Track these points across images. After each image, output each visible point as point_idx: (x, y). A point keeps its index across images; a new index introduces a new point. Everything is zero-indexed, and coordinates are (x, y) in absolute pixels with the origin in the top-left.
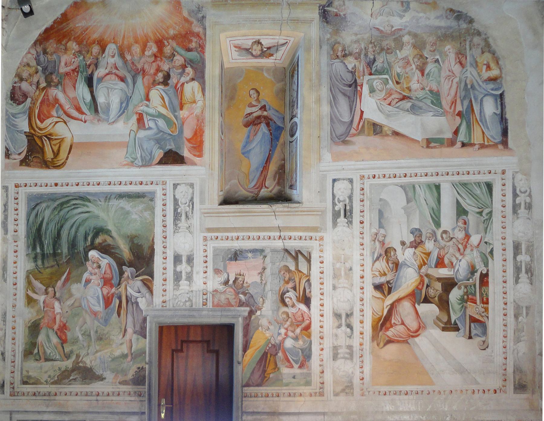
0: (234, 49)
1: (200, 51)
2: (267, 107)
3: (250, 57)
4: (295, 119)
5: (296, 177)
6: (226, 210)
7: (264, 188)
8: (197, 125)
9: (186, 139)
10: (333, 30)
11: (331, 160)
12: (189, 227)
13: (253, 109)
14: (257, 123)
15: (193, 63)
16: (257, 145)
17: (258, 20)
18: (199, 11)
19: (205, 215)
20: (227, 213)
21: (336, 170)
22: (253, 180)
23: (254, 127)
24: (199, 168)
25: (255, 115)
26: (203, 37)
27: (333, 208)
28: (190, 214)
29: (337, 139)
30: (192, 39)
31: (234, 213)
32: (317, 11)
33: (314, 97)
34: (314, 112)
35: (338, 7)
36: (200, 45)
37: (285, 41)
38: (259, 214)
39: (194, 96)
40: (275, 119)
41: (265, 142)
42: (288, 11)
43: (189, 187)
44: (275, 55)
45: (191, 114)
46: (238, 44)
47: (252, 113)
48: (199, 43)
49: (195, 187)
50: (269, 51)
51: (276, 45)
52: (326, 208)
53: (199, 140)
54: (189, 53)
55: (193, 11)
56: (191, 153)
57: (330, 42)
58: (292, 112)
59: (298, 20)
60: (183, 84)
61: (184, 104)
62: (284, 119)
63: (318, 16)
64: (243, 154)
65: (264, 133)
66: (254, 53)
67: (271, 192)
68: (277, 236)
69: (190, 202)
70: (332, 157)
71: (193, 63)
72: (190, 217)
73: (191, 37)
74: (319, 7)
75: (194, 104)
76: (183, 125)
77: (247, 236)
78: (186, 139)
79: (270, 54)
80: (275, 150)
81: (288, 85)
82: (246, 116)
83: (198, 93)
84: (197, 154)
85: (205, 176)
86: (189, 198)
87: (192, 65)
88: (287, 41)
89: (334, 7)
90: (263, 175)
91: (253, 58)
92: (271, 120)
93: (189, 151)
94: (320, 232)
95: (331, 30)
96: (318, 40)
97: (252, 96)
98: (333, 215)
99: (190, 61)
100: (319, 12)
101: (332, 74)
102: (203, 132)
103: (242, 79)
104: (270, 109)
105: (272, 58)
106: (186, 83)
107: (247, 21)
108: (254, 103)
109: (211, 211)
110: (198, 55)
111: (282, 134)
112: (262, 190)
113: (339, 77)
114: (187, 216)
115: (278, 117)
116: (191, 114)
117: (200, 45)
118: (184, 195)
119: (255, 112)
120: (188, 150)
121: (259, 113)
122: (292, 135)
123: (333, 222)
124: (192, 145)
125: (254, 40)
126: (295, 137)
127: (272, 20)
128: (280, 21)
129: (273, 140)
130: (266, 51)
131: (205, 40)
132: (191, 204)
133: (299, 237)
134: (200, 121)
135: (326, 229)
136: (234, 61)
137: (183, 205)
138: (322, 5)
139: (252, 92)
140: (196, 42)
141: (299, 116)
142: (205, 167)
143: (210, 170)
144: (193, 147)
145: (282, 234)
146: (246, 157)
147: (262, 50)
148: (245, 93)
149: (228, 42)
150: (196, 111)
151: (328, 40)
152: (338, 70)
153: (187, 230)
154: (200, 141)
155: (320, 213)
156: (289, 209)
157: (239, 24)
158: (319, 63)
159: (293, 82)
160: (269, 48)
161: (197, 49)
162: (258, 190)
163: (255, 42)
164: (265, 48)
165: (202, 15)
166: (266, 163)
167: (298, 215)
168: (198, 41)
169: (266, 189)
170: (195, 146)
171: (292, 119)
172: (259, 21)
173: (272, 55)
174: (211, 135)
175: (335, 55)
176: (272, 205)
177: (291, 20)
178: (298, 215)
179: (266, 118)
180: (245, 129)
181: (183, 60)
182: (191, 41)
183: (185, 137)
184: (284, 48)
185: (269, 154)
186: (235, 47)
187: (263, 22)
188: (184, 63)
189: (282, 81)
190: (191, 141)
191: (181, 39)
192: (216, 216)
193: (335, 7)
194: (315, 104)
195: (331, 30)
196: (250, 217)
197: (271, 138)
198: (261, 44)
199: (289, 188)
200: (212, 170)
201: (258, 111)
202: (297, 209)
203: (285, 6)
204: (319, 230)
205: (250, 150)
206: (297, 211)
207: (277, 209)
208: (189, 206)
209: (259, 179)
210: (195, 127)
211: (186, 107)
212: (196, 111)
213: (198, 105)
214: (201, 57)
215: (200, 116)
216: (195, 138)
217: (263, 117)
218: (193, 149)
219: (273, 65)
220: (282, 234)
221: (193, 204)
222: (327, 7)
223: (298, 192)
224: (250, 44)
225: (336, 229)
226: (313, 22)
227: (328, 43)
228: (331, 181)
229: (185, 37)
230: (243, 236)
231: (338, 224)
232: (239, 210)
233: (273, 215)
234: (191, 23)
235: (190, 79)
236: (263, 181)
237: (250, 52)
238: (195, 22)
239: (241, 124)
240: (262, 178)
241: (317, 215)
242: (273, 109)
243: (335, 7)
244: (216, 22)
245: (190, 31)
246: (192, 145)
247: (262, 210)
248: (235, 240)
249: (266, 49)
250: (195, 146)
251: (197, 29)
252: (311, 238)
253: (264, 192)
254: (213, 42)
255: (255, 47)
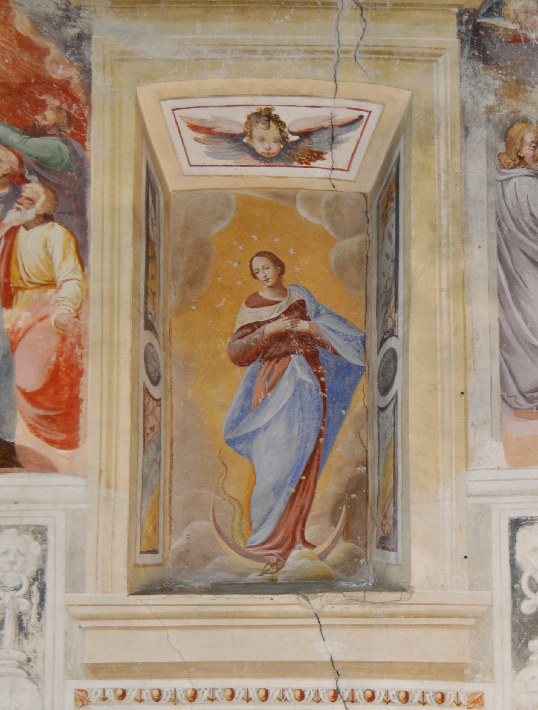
0: (189, 135)
1: (72, 135)
2: (310, 308)
3: (248, 159)
4: (392, 343)
5: (395, 511)
6: (155, 610)
7: (299, 545)
8: (60, 353)
9: (24, 393)
10: (505, 82)
11: (502, 461)
12: (29, 660)
13: (265, 313)
14: (277, 353)
15: (49, 171)
16: (277, 416)
17: (260, 49)
18: (69, 18)
19: (84, 624)
20: (158, 617)
21: (522, 493)
22: (261, 524)
23: (266, 367)
24: (66, 479)
25: (269, 329)
26: (81, 95)
27: (515, 606)
28: (31, 621)
29: (521, 400)
30: (44, 101)
31: (180, 617)
32: (453, 28)
33: (444, 276)
34: (445, 317)
35: (522, 17)
36: (70, 117)
37: (355, 115)
38: (269, 622)
39: (50, 266)
40: (337, 343)
41: (302, 409)
42: (358, 26)
43: (29, 537)
44: (327, 156)
45: (42, 319)
46: (202, 120)
47: (259, 324)
48: (68, 114)
49: (50, 536)
50: (305, 144)
51: (328, 124)
52: (491, 606)
53: (66, 396)
54: (35, 140)
55: (48, 19)
56: (38, 436)
57: (496, 117)
58: (385, 322)
59: (390, 53)
60: (13, 232)
61: (18, 288)
62: (364, 343)
63: (457, 41)
64: (231, 443)
65: (300, 384)
66: (260, 148)
67: (322, 557)
68: (328, 691)
69: (31, 584)
70: (507, 453)
71: (49, 171)
72: (30, 629)
73: (41, 94)
74: (460, 15)
75: (50, 292)
76: (13, 351)
77: (225, 690)
78: (24, 393)
79: (312, 152)
80: (335, 431)
81: (374, 243)
82: (240, 333)
83: (64, 258)
84: (62, 437)
85: (84, 506)
86: (31, 570)
87: (44, 174)
88: (361, 113)
89: (506, 17)
90: (296, 510)
91: (257, 162)
92: (323, 345)
93: (33, 429)
94: (472, 679)
95: (498, 83)
96: (458, 114)
97: (260, 276)
98: (515, 628)
99: (37, 163)
100: (459, 32)
101: (505, 210)
102: (81, 373)
103: (225, 224)
104: (317, 314)
105: (318, 163)
106: (22, 230)
107: (225, 51)
108: (266, 294)
109: (106, 611)
110: (65, 148)
111: (359, 387)
112: (295, 553)
113: (528, 218)
114: (21, 627)
115: (346, 338)
116: (42, 319)
117: (70, 117)
118: (13, 563)
119: (269, 322)
120: (30, 425)
121: (284, 324)
122: (385, 390)
123: (513, 649)
124: (41, 412)
125: (254, 110)
126: (391, 394)
127: (306, 52)
128: (332, 53)
129: (328, 405)
130: (296, 142)
131: (88, 103)
132: (35, 588)
133: (402, 695)
134: (70, 340)
135: (492, 671)
136: (196, 171)
137: (10, 594)
138: (467, 11)
139: (259, 263)
140: (59, 108)
141: (400, 333)
142: (85, 477)
143: (103, 486)
144: (45, 417)
145: (344, 684)
146: (240, 453)
147: (284, 139)
148: (235, 265)
149: (168, 114)
150: (57, 312)
151: (490, 110)
152: (523, 200)
153: (20, 671)
154: (70, 398)
155: (471, 622)
156: (367, 609)
157: (197, 59)
158: (463, 178)
159: (386, 233)
160: (306, 134)
161: (60, 131)
162: (280, 551)
163: (258, 115)
164: (293, 134)
165: (77, 31)
166: (307, 472)
167: (396, 626)
168: (65, 107)
169: (306, 550)
170: (51, 413)
171: (383, 341)
172: (265, 52)
173: (319, 156)
174: (105, 381)
175: (514, 155)
176: (310, 596)
177: (369, 52)
178: (396, 626)
179: (303, 337)
180: (238, 369)
181: (13, 158)
182: (43, 106)
183: (19, 388)
184: (353, 135)
185: (318, 444)
186: (194, 128)
187: (276, 56)
188: (16, 167)
189: (358, 231)
190: (40, 399)
191: (9, 99)
192: (120, 628)
193: (512, 16)
194: (448, 296)
195: (498, 83)
196: (237, 632)
197: (324, 399)
198: (276, 120)
199: (378, 547)
200: (108, 486)
201: (279, 317)
202: (392, 609)
203: (347, 12)
204: (467, 672)
205: (255, 433)
206: (392, 616)
207: (328, 609)
208: (29, 595)
209: (284, 516)
210: (54, 359)
211: (22, 298)
212: (57, 312)
213: (63, 293)
214: (74, 153)
215: (71, 327)
216: (51, 391)
217: (295, 338)
218: (44, 423)
219: (327, 185)
220: (344, 684)
221: (42, 591)
222: (484, 15)
223: (400, 557)
224: (243, 119)
225: (526, 673)
226: (441, 60)
227: (489, 120)
228: (505, 526)
229: (20, 92)
230: (213, 690)
231: (532, 658)
232: (199, 609)
233: (312, 626)
234: (43, 53)
235: (38, 216)
236: (296, 523)
237: (246, 145)
238: (55, 52)
239: (224, 355)
240: (292, 517)
241: (460, 626)
242: (330, 313)
243: (512, 16)
244: (123, 52)
245: (37, 77)
246: (41, 412)
247: (275, 609)
248: (184, 701)
249: (296, 138)
250: (51, 413)
251: (60, 72)
252: (232, 696)
253: (299, 559)
254: (112, 108)
255: (259, 130)
